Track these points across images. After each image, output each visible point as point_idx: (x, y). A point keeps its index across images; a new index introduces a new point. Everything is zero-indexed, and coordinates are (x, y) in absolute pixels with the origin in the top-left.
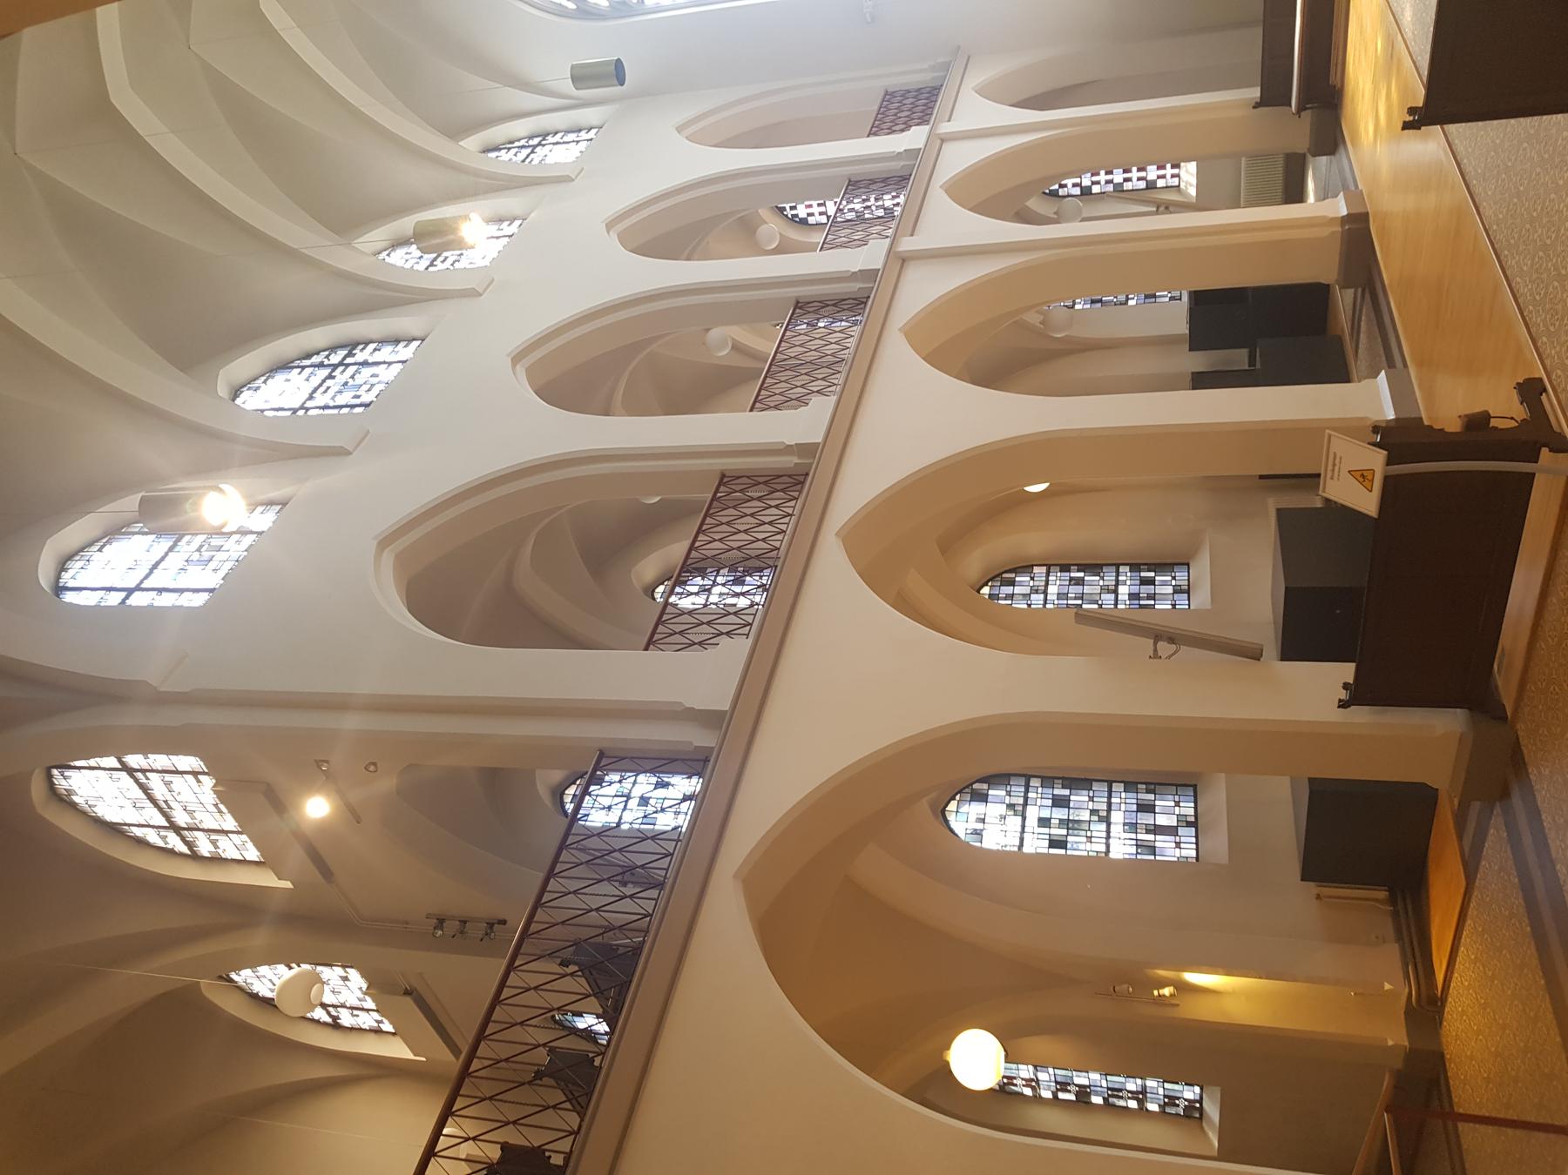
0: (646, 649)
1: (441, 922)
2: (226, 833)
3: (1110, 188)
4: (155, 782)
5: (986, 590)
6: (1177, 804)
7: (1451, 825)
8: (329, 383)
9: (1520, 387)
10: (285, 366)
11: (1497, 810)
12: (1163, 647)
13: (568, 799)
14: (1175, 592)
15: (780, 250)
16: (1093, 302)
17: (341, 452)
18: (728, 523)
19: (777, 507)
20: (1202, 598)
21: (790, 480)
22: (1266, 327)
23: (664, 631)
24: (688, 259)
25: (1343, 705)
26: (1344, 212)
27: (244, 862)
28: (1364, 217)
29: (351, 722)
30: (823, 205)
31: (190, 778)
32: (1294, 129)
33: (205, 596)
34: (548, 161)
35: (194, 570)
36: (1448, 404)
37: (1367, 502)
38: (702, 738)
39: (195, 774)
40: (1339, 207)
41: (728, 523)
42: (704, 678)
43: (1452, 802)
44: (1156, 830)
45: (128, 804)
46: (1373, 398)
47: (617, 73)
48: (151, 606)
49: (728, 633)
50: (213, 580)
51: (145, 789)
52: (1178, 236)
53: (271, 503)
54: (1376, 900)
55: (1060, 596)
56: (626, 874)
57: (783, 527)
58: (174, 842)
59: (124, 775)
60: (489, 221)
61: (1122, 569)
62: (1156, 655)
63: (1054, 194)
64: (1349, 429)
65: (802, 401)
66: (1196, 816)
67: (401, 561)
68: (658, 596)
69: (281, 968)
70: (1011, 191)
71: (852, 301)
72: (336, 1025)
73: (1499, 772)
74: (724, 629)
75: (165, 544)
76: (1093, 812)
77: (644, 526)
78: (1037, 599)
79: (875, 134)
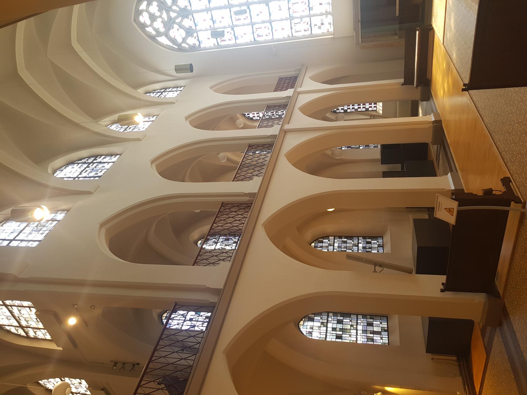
0: (193, 265)
1: (116, 364)
2: (40, 329)
3: (353, 110)
4: (15, 310)
5: (313, 244)
6: (381, 323)
7: (480, 334)
8: (87, 169)
9: (502, 180)
10: (72, 163)
11: (498, 329)
12: (378, 269)
13: (164, 318)
14: (378, 247)
15: (244, 128)
16: (348, 147)
17: (89, 193)
18: (224, 220)
19: (241, 214)
20: (388, 249)
21: (246, 205)
22: (407, 157)
23: (201, 258)
24: (213, 130)
25: (442, 291)
26: (433, 119)
27: (45, 340)
28: (440, 121)
29: (86, 290)
30: (258, 113)
31: (28, 309)
32: (415, 92)
33: (37, 243)
34: (167, 97)
35: (34, 234)
36: (476, 185)
37: (452, 220)
38: (212, 299)
39: (29, 307)
40: (432, 118)
41: (224, 220)
42: (214, 276)
43: (480, 325)
44: (374, 333)
45: (5, 317)
46: (447, 182)
47: (191, 68)
49: (223, 260)
50: (41, 237)
51: (11, 312)
52: (356, 128)
53: (63, 210)
54: (453, 360)
55: (339, 247)
56: (184, 348)
57: (243, 222)
58: (21, 332)
59: (4, 307)
60: (145, 116)
61: (360, 238)
62: (375, 271)
63: (335, 112)
64: (443, 193)
65: (251, 178)
66: (388, 327)
67: (108, 232)
68: (198, 244)
69: (58, 379)
70: (320, 110)
71: (268, 145)
73: (498, 316)
74: (222, 258)
75: (25, 224)
76: (352, 326)
77: (194, 220)
78: (331, 248)
79: (276, 91)
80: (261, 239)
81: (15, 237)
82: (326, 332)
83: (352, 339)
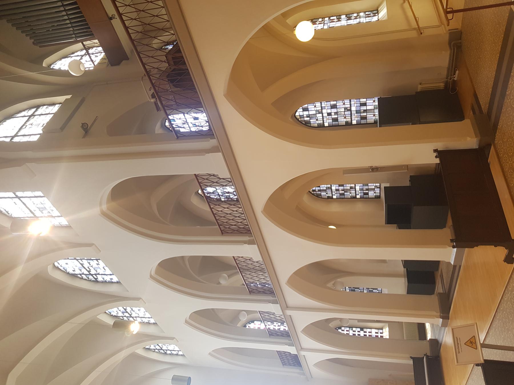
48: (23, 191)
72: (96, 281)
80: (293, 297)
81: (17, 133)
82: (323, 118)
83: (348, 120)
